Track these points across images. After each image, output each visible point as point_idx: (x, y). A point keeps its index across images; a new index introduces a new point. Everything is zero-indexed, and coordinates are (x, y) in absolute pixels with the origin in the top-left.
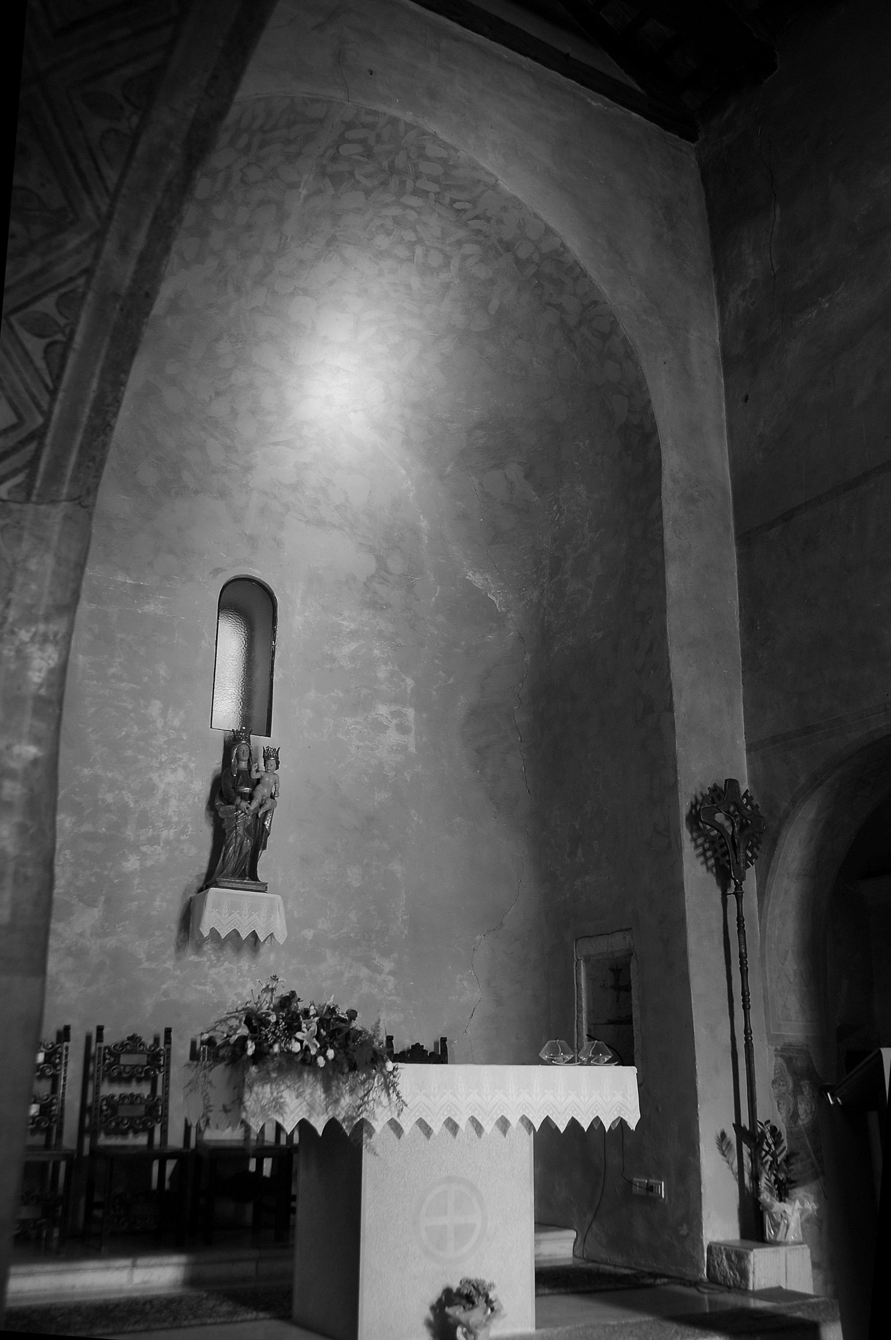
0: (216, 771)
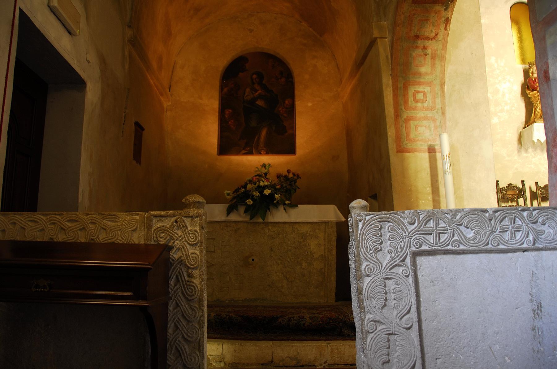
0: (522, 81)
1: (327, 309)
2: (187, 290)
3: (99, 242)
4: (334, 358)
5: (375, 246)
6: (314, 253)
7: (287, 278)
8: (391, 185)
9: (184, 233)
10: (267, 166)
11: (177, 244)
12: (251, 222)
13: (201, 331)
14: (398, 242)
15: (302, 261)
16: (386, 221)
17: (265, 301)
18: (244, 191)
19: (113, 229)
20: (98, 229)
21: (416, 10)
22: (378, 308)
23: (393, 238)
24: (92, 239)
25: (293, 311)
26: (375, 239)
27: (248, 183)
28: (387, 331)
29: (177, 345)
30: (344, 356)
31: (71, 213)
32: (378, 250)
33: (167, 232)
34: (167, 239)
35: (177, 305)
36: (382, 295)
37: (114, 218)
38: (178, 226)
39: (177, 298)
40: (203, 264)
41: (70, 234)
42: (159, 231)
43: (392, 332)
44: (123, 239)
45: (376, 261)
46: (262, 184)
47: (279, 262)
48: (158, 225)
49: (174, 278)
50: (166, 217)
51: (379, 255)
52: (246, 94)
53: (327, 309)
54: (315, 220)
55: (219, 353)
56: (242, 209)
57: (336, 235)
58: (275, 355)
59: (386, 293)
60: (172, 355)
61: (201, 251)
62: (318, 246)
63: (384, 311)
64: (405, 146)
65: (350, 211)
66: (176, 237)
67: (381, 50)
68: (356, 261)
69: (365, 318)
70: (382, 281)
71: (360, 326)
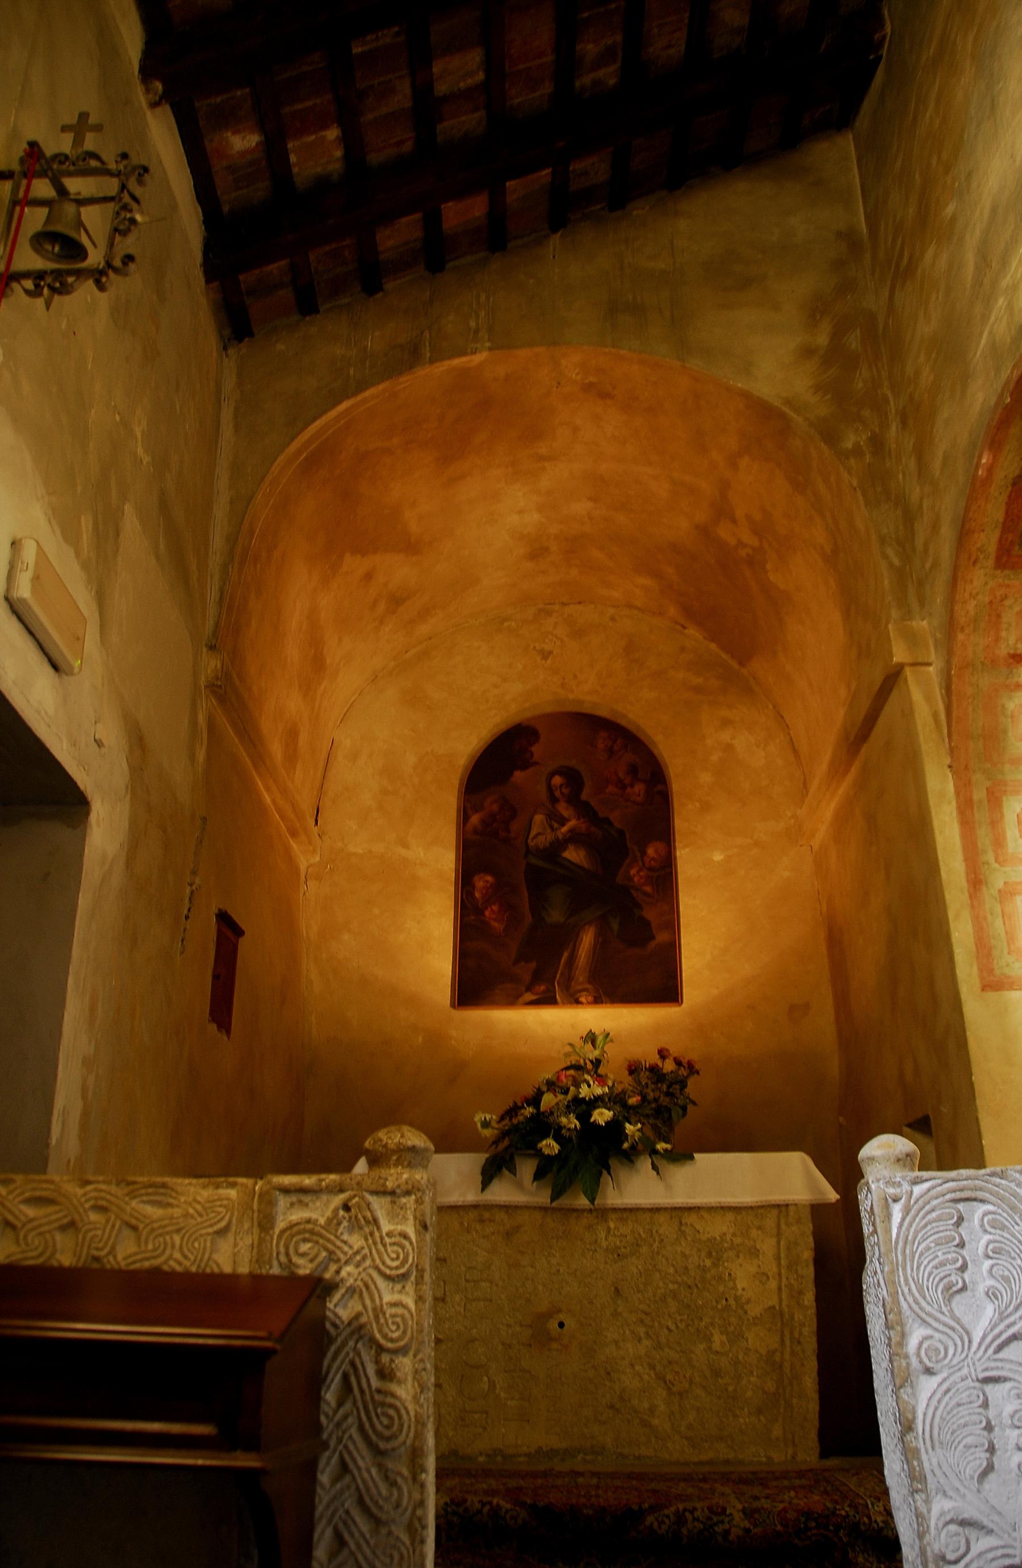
1: (797, 1482)
5: (945, 1277)
6: (748, 1301)
9: (370, 1241)
10: (600, 1040)
12: (553, 1209)
13: (417, 1552)
15: (711, 1328)
16: (975, 1200)
17: (599, 1458)
18: (532, 1114)
20: (113, 1226)
21: (1008, 586)
22: (968, 1477)
23: (998, 1251)
24: (97, 1259)
25: (690, 1490)
26: (944, 1254)
27: (544, 1088)
32: (955, 1289)
35: (344, 1468)
36: (976, 1436)
37: (162, 1194)
39: (346, 1447)
40: (426, 1339)
45: (953, 1323)
46: (584, 1092)
47: (641, 1330)
51: (959, 1304)
52: (533, 833)
53: (797, 1482)
54: (747, 1199)
56: (527, 1168)
57: (812, 1244)
62: (761, 1282)
64: (1006, 971)
66: (345, 1253)
67: (917, 696)
68: (888, 1326)
69: (929, 1511)
70: (974, 1388)
71: (917, 1540)
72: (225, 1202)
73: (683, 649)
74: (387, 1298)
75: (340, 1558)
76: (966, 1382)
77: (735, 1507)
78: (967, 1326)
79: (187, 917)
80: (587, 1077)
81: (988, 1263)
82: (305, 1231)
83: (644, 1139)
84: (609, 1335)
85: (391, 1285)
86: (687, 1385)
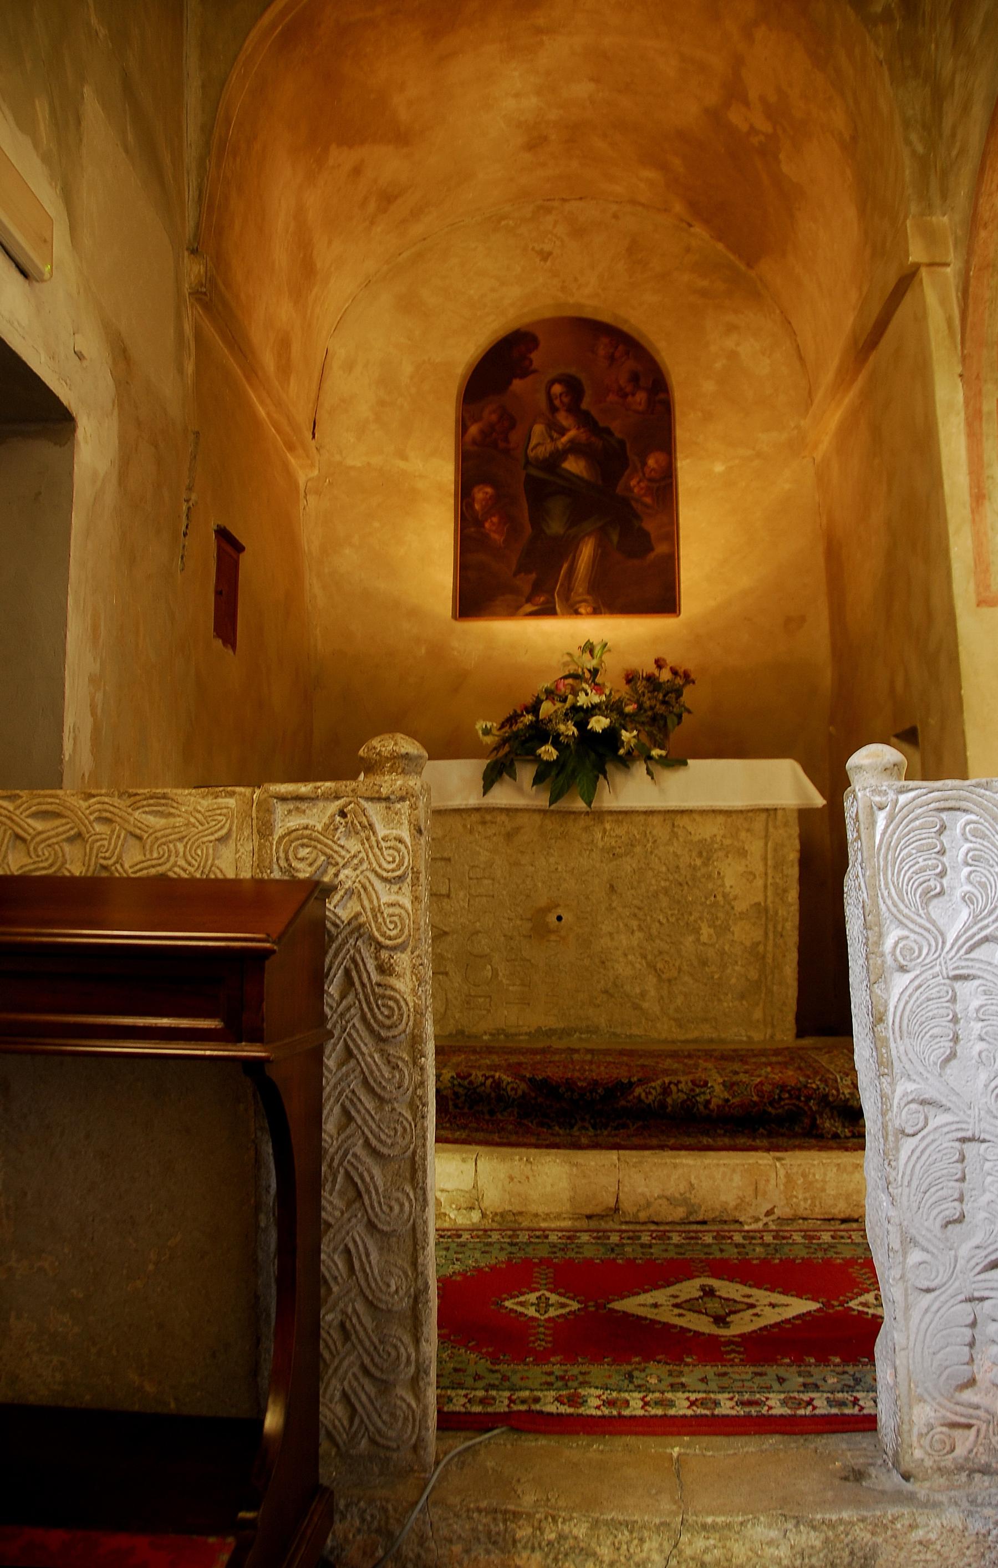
1: (774, 1059)
2: (376, 1010)
3: (125, 875)
4: (795, 1200)
5: (925, 882)
6: (735, 898)
7: (656, 970)
8: (960, 699)
9: (367, 845)
10: (597, 651)
11: (347, 877)
12: (552, 811)
14: (992, 870)
16: (959, 809)
17: (594, 1036)
19: (163, 836)
20: (119, 837)
22: (931, 1063)
24: (105, 868)
25: (676, 1066)
26: (925, 860)
27: (543, 697)
28: (957, 1130)
29: (350, 1168)
30: (823, 1194)
31: (42, 792)
32: (933, 893)
33: (316, 843)
34: (316, 865)
35: (349, 1054)
36: (943, 1027)
38: (349, 824)
39: (350, 1035)
40: (423, 937)
41: (40, 853)
42: (292, 842)
43: (973, 1135)
44: (190, 864)
45: (928, 925)
46: (582, 700)
47: (634, 924)
48: (291, 824)
49: (338, 976)
50: (312, 799)
51: (936, 910)
52: (533, 442)
53: (774, 1059)
54: (738, 803)
55: (466, 1183)
56: (526, 773)
57: (798, 847)
58: (626, 1189)
59: (955, 1020)
60: (334, 1194)
61: (416, 898)
63: (948, 1071)
65: (851, 779)
66: (343, 858)
67: (931, 297)
68: (866, 927)
69: (894, 1092)
71: (880, 1116)
72: (225, 811)
73: (688, 250)
74: (384, 899)
75: (348, 1131)
76: (937, 979)
77: (716, 1081)
78: (942, 928)
79: (185, 534)
80: (585, 686)
81: (967, 870)
82: (303, 837)
83: (640, 745)
84: (604, 927)
85: (388, 886)
86: (676, 974)
